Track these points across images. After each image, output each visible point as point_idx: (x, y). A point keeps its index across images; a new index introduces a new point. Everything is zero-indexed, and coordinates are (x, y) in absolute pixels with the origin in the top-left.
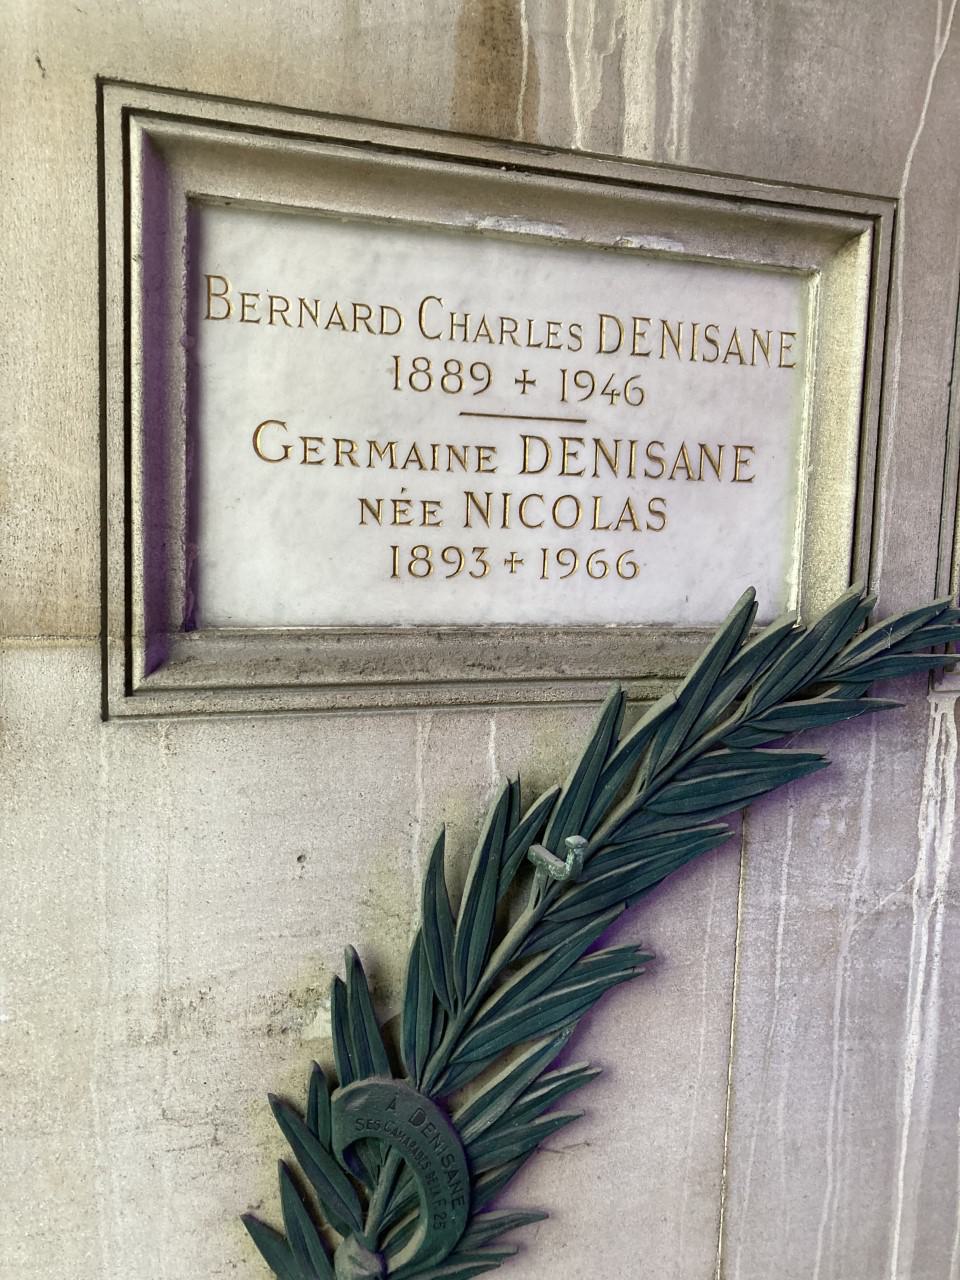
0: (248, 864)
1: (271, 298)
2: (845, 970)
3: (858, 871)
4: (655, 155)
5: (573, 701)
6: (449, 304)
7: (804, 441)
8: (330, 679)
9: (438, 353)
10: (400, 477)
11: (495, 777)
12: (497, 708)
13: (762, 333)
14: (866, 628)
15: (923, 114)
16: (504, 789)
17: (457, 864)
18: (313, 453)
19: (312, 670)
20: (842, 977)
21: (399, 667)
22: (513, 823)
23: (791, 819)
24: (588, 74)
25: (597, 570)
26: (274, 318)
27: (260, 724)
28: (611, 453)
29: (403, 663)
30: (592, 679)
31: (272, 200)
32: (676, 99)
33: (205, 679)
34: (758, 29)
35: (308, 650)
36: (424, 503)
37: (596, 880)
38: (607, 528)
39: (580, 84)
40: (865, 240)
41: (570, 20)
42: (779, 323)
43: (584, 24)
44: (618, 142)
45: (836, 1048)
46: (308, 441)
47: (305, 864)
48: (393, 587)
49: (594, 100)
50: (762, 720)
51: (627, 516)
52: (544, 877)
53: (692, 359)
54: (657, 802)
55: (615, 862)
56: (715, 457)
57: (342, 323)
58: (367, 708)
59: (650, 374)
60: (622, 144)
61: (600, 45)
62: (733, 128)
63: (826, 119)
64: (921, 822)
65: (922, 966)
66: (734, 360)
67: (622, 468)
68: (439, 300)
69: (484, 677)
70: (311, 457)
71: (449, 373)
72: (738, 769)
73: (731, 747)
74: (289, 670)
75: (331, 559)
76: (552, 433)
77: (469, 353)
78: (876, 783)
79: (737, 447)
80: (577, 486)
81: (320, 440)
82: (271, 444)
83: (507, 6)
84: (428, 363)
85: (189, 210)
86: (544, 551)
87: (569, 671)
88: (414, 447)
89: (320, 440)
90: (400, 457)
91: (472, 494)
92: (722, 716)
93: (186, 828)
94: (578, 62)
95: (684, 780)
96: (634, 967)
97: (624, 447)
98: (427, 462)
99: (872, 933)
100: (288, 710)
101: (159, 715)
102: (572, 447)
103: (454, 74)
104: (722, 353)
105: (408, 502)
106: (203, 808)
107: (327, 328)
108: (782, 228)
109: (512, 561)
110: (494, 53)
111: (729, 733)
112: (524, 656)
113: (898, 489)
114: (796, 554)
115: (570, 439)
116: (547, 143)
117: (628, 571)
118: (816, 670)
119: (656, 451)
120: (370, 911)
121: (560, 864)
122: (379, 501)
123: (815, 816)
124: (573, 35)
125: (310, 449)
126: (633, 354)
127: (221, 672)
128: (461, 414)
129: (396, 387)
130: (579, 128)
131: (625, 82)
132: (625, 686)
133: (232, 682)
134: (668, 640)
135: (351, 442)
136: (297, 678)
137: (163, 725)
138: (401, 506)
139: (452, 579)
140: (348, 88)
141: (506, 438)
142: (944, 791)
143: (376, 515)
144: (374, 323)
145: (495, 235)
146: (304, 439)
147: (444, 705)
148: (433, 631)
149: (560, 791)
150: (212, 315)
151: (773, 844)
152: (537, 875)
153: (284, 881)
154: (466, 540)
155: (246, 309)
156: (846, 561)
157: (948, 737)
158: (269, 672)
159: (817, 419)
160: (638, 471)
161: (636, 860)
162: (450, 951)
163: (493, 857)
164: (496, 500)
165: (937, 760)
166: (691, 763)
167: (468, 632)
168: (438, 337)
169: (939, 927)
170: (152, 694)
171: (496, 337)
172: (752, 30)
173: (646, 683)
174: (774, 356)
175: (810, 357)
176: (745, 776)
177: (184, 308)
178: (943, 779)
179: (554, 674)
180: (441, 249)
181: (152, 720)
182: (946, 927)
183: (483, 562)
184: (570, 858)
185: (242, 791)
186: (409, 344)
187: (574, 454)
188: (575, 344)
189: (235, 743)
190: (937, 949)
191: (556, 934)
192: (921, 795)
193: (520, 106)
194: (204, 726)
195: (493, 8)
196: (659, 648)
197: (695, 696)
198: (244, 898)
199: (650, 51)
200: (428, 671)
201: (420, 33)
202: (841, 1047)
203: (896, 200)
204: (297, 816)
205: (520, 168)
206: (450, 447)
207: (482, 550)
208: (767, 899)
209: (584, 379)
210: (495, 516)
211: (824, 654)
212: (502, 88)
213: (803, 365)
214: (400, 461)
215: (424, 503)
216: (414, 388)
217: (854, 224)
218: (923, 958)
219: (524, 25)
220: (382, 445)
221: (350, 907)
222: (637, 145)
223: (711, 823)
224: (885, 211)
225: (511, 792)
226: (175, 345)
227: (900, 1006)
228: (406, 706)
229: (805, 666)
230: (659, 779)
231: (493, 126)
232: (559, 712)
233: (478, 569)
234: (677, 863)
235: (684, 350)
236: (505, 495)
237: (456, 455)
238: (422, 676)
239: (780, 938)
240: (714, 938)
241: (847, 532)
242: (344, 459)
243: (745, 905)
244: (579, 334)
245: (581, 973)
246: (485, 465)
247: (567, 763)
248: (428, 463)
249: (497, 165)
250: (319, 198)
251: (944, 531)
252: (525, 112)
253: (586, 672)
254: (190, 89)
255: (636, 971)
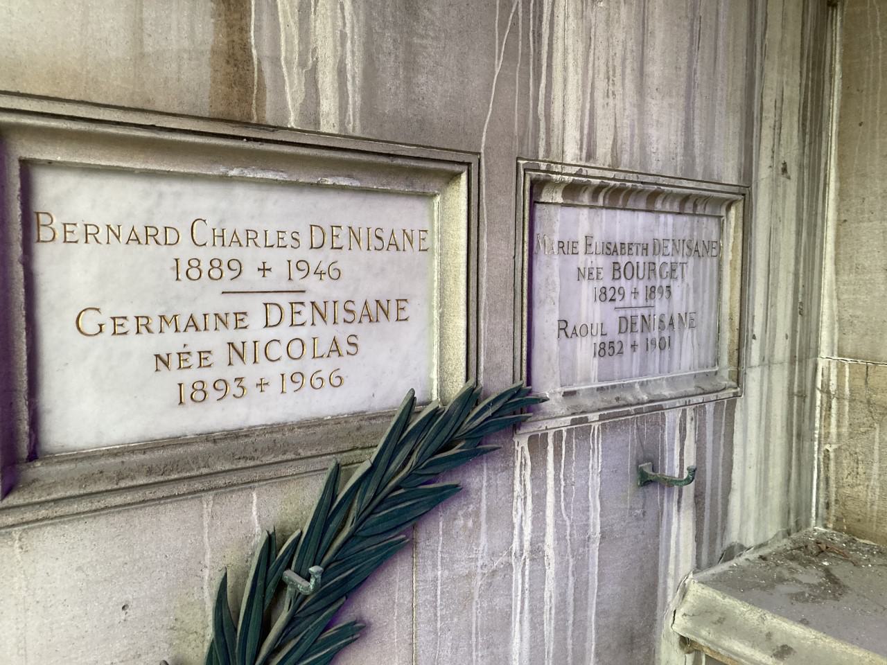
0: (85, 619)
1: (86, 225)
2: (477, 609)
3: (481, 548)
4: (340, 130)
5: (306, 472)
6: (211, 223)
7: (436, 293)
8: (141, 482)
9: (205, 255)
10: (182, 338)
11: (258, 529)
12: (256, 484)
13: (408, 231)
14: (477, 405)
15: (491, 105)
16: (265, 539)
17: (235, 591)
18: (120, 327)
19: (127, 477)
20: (476, 615)
21: (187, 466)
22: (272, 559)
23: (441, 524)
24: (296, 82)
25: (317, 383)
26: (89, 239)
27: (91, 520)
28: (323, 310)
29: (191, 462)
30: (317, 456)
31: (84, 162)
32: (350, 96)
33: (48, 495)
34: (396, 56)
35: (123, 462)
36: (200, 353)
37: (327, 585)
38: (322, 356)
39: (291, 87)
40: (464, 177)
41: (283, 49)
42: (418, 226)
43: (292, 52)
44: (317, 123)
45: (474, 657)
46: (117, 320)
47: (127, 610)
48: (180, 411)
49: (300, 97)
50: (423, 468)
51: (334, 348)
52: (294, 590)
53: (368, 249)
54: (362, 530)
55: (338, 571)
56: (385, 307)
57: (138, 240)
58: (168, 497)
59: (344, 260)
60: (319, 124)
61: (302, 64)
62: (385, 114)
63: (438, 108)
64: (514, 513)
65: (519, 598)
66: (393, 248)
67: (330, 318)
68: (204, 221)
69: (247, 465)
70: (119, 330)
71: (213, 267)
72: (410, 500)
73: (405, 488)
74: (110, 479)
75: (136, 397)
76: (284, 300)
77: (226, 254)
78: (489, 493)
79: (397, 300)
80: (302, 332)
81: (125, 318)
82: (89, 324)
83: (242, 40)
84: (199, 261)
85: (21, 170)
86: (283, 375)
87: (303, 454)
88: (191, 317)
89: (125, 318)
90: (182, 322)
91: (232, 344)
92: (399, 471)
93: (38, 602)
94: (289, 72)
95: (379, 512)
96: (353, 635)
97: (330, 305)
98: (201, 326)
99: (491, 583)
100: (112, 507)
101: (13, 526)
102: (297, 308)
103: (210, 82)
104: (386, 245)
105: (188, 353)
106: (49, 586)
107: (127, 243)
108: (417, 171)
109: (261, 385)
110: (236, 69)
111: (403, 480)
112: (272, 448)
113: (490, 320)
114: (435, 361)
115: (295, 303)
116: (272, 124)
117: (337, 381)
118: (452, 434)
119: (350, 306)
120: (176, 633)
121: (305, 583)
122: (168, 355)
123: (455, 519)
124: (286, 58)
125: (118, 325)
126: (332, 248)
127: (59, 487)
128: (223, 293)
129: (177, 279)
130: (292, 114)
131: (319, 86)
132: (339, 458)
133: (68, 494)
134: (363, 423)
135: (147, 318)
136: (117, 484)
137: (16, 533)
138: (184, 357)
139: (221, 401)
140: (137, 90)
141: (254, 306)
142: (525, 492)
143: (166, 364)
144: (160, 238)
145: (240, 179)
146: (114, 319)
147: (221, 488)
148: (208, 437)
149: (302, 533)
150: (41, 239)
151: (432, 541)
152: (289, 589)
153: (113, 625)
154: (230, 375)
155: (67, 234)
156: (464, 364)
157: (525, 460)
158: (96, 482)
159: (442, 282)
160: (340, 320)
161: (352, 567)
162: (234, 650)
163: (260, 583)
164: (249, 346)
165: (521, 475)
166: (382, 502)
167: (234, 435)
168: (205, 244)
169: (527, 573)
170: (7, 511)
171: (244, 242)
172: (393, 56)
173: (352, 453)
174: (416, 243)
175: (437, 245)
176: (413, 505)
177: (21, 238)
178: (525, 485)
179: (293, 456)
180: (203, 188)
181: (8, 530)
182: (531, 572)
183: (242, 387)
184: (313, 581)
185: (79, 569)
186: (185, 250)
187: (299, 313)
188: (295, 244)
189: (73, 536)
190: (527, 586)
191: (303, 624)
192: (513, 497)
193: (254, 101)
194: (48, 528)
195: (233, 41)
196: (358, 429)
197: (383, 461)
198: (83, 643)
199: (333, 68)
200: (209, 467)
201: (186, 56)
202: (477, 656)
203: (480, 154)
204: (121, 579)
205: (256, 140)
206: (216, 315)
207: (241, 379)
208: (430, 575)
209: (302, 266)
210: (249, 357)
211: (479, 179)
212: (242, 90)
213: (433, 248)
214: (182, 327)
215: (200, 353)
216: (190, 278)
217: (457, 168)
218: (520, 593)
219: (254, 52)
220: (169, 317)
221: (162, 633)
222: (329, 124)
223: (396, 536)
224: (473, 160)
225: (271, 543)
226: (15, 264)
227: (509, 623)
228: (195, 492)
229: (445, 432)
230: (363, 515)
231: (237, 115)
232: (297, 481)
233: (239, 392)
234: (374, 566)
235: (363, 244)
236: (255, 342)
237: (221, 319)
238: (205, 471)
239: (439, 597)
240: (400, 605)
241: (463, 347)
242: (143, 329)
243: (417, 581)
244: (297, 238)
245: (320, 645)
246: (240, 324)
247: (304, 513)
248: (201, 326)
249: (241, 138)
250: (119, 160)
251: (516, 341)
252: (257, 105)
253: (314, 452)
254: (21, 92)
255: (355, 637)
